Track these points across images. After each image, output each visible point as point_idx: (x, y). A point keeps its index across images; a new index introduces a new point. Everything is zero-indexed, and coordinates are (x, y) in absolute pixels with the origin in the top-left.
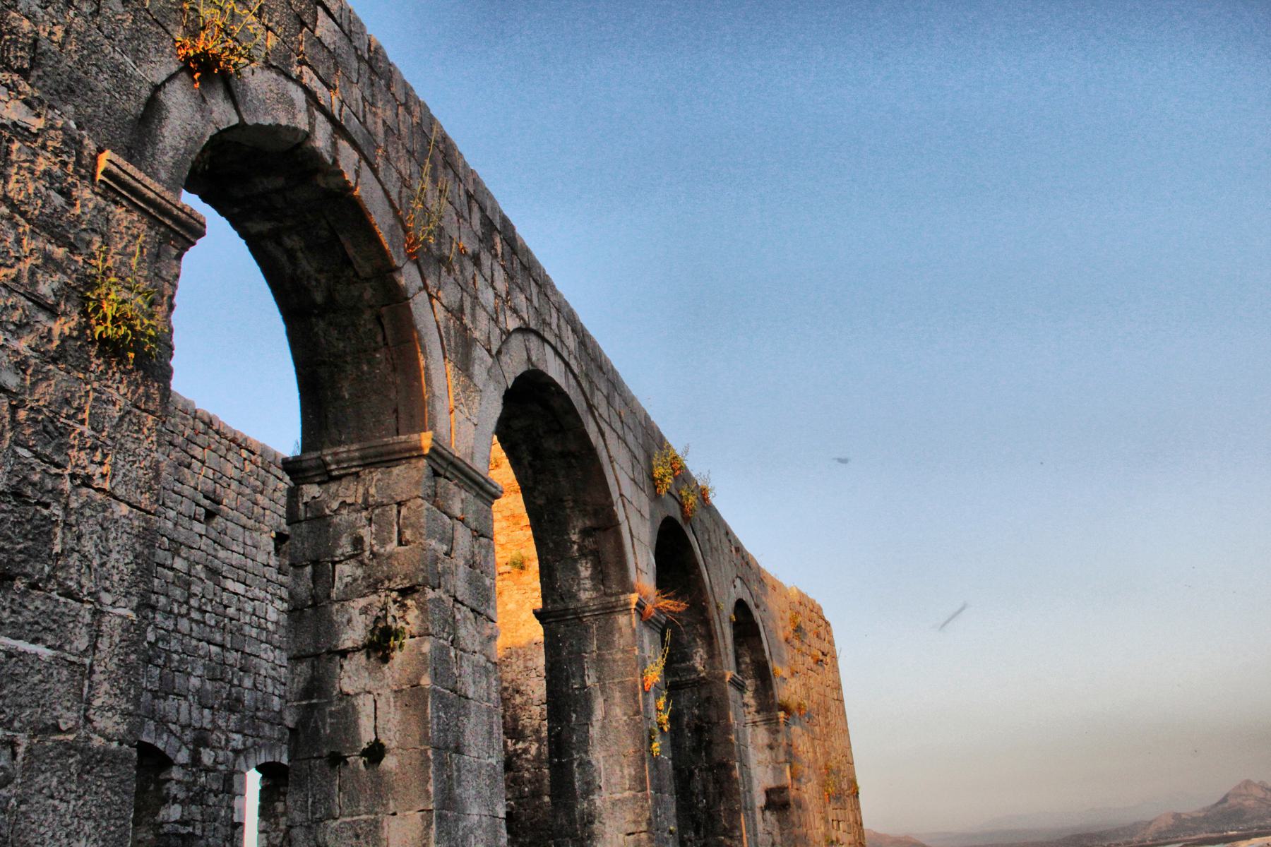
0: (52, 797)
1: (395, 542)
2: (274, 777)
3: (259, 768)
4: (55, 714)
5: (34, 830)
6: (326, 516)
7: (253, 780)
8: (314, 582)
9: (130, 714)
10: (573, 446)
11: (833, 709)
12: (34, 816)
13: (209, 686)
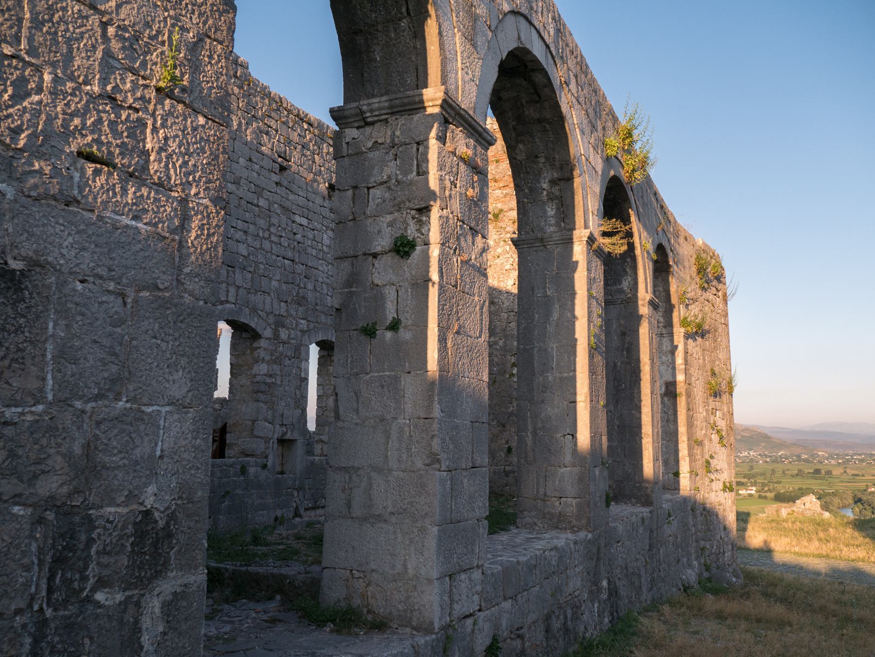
0: (155, 337)
1: (415, 173)
2: (326, 347)
3: (318, 344)
4: (154, 275)
5: (143, 360)
6: (362, 153)
7: (314, 351)
8: (354, 202)
9: (212, 281)
10: (548, 115)
11: (720, 330)
12: (143, 351)
13: (284, 287)
